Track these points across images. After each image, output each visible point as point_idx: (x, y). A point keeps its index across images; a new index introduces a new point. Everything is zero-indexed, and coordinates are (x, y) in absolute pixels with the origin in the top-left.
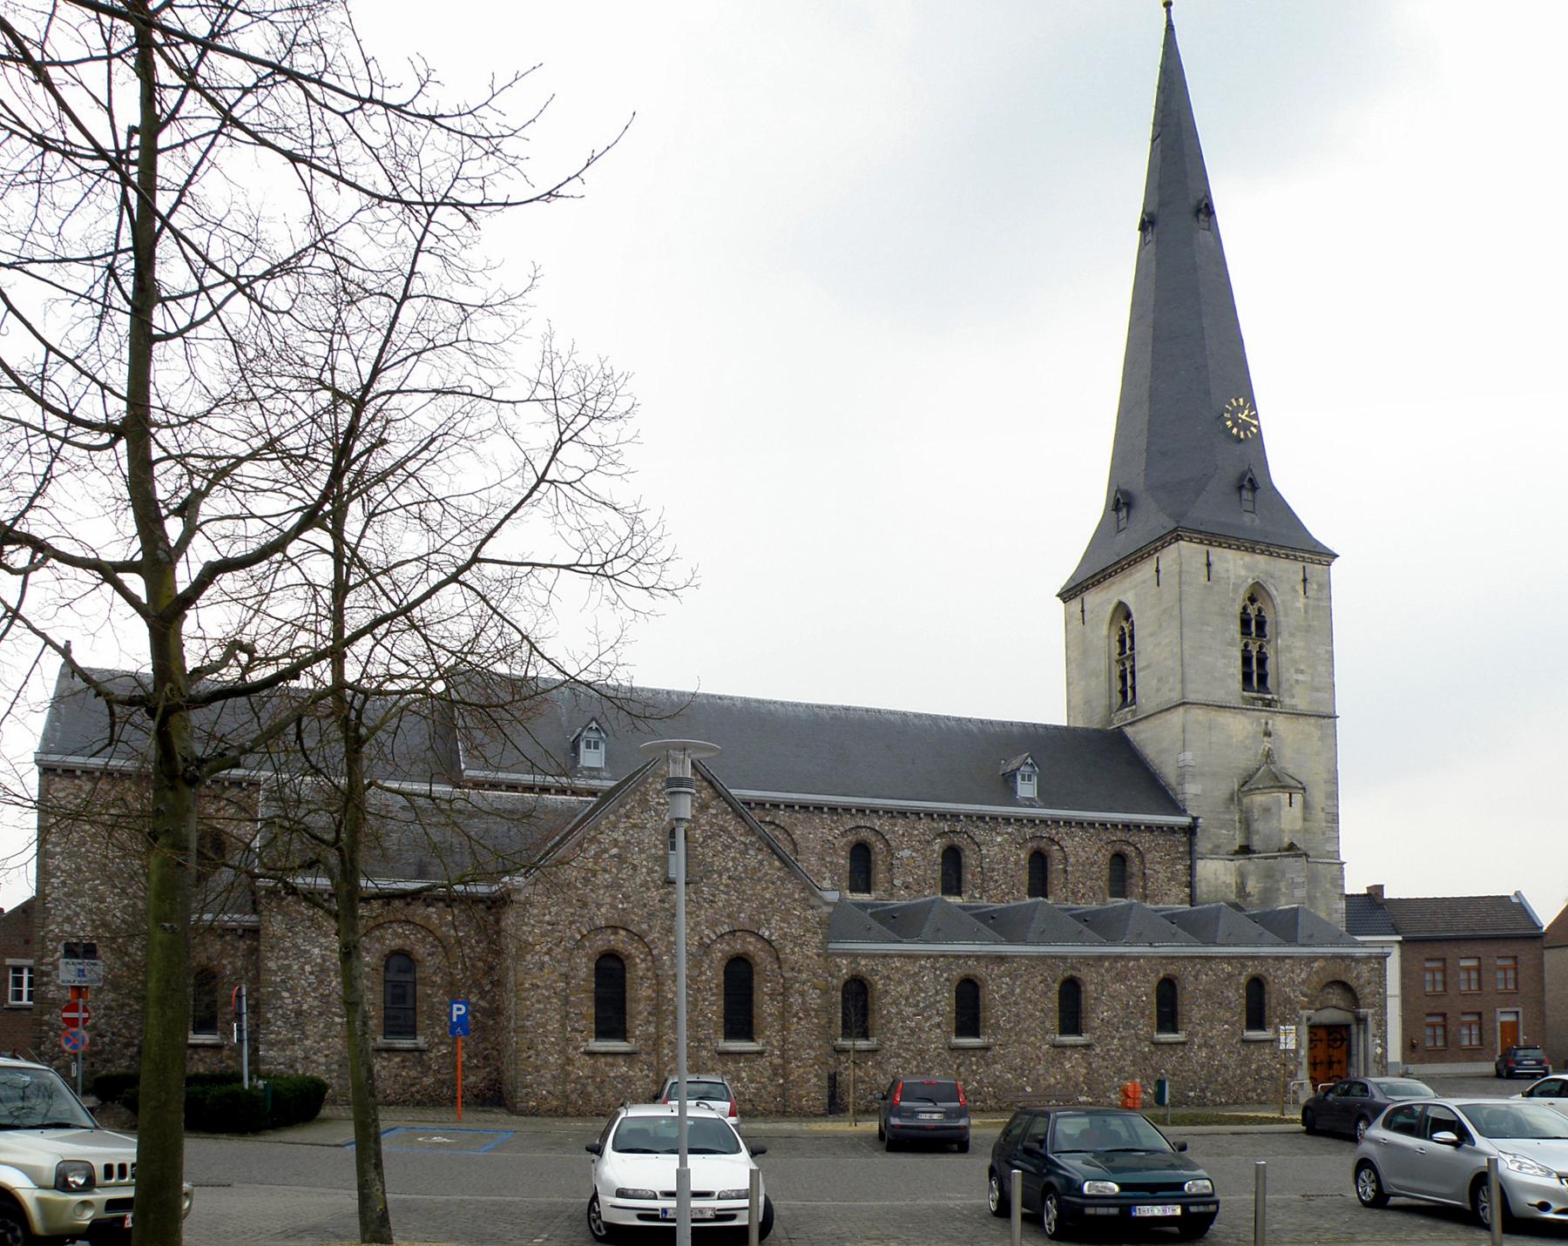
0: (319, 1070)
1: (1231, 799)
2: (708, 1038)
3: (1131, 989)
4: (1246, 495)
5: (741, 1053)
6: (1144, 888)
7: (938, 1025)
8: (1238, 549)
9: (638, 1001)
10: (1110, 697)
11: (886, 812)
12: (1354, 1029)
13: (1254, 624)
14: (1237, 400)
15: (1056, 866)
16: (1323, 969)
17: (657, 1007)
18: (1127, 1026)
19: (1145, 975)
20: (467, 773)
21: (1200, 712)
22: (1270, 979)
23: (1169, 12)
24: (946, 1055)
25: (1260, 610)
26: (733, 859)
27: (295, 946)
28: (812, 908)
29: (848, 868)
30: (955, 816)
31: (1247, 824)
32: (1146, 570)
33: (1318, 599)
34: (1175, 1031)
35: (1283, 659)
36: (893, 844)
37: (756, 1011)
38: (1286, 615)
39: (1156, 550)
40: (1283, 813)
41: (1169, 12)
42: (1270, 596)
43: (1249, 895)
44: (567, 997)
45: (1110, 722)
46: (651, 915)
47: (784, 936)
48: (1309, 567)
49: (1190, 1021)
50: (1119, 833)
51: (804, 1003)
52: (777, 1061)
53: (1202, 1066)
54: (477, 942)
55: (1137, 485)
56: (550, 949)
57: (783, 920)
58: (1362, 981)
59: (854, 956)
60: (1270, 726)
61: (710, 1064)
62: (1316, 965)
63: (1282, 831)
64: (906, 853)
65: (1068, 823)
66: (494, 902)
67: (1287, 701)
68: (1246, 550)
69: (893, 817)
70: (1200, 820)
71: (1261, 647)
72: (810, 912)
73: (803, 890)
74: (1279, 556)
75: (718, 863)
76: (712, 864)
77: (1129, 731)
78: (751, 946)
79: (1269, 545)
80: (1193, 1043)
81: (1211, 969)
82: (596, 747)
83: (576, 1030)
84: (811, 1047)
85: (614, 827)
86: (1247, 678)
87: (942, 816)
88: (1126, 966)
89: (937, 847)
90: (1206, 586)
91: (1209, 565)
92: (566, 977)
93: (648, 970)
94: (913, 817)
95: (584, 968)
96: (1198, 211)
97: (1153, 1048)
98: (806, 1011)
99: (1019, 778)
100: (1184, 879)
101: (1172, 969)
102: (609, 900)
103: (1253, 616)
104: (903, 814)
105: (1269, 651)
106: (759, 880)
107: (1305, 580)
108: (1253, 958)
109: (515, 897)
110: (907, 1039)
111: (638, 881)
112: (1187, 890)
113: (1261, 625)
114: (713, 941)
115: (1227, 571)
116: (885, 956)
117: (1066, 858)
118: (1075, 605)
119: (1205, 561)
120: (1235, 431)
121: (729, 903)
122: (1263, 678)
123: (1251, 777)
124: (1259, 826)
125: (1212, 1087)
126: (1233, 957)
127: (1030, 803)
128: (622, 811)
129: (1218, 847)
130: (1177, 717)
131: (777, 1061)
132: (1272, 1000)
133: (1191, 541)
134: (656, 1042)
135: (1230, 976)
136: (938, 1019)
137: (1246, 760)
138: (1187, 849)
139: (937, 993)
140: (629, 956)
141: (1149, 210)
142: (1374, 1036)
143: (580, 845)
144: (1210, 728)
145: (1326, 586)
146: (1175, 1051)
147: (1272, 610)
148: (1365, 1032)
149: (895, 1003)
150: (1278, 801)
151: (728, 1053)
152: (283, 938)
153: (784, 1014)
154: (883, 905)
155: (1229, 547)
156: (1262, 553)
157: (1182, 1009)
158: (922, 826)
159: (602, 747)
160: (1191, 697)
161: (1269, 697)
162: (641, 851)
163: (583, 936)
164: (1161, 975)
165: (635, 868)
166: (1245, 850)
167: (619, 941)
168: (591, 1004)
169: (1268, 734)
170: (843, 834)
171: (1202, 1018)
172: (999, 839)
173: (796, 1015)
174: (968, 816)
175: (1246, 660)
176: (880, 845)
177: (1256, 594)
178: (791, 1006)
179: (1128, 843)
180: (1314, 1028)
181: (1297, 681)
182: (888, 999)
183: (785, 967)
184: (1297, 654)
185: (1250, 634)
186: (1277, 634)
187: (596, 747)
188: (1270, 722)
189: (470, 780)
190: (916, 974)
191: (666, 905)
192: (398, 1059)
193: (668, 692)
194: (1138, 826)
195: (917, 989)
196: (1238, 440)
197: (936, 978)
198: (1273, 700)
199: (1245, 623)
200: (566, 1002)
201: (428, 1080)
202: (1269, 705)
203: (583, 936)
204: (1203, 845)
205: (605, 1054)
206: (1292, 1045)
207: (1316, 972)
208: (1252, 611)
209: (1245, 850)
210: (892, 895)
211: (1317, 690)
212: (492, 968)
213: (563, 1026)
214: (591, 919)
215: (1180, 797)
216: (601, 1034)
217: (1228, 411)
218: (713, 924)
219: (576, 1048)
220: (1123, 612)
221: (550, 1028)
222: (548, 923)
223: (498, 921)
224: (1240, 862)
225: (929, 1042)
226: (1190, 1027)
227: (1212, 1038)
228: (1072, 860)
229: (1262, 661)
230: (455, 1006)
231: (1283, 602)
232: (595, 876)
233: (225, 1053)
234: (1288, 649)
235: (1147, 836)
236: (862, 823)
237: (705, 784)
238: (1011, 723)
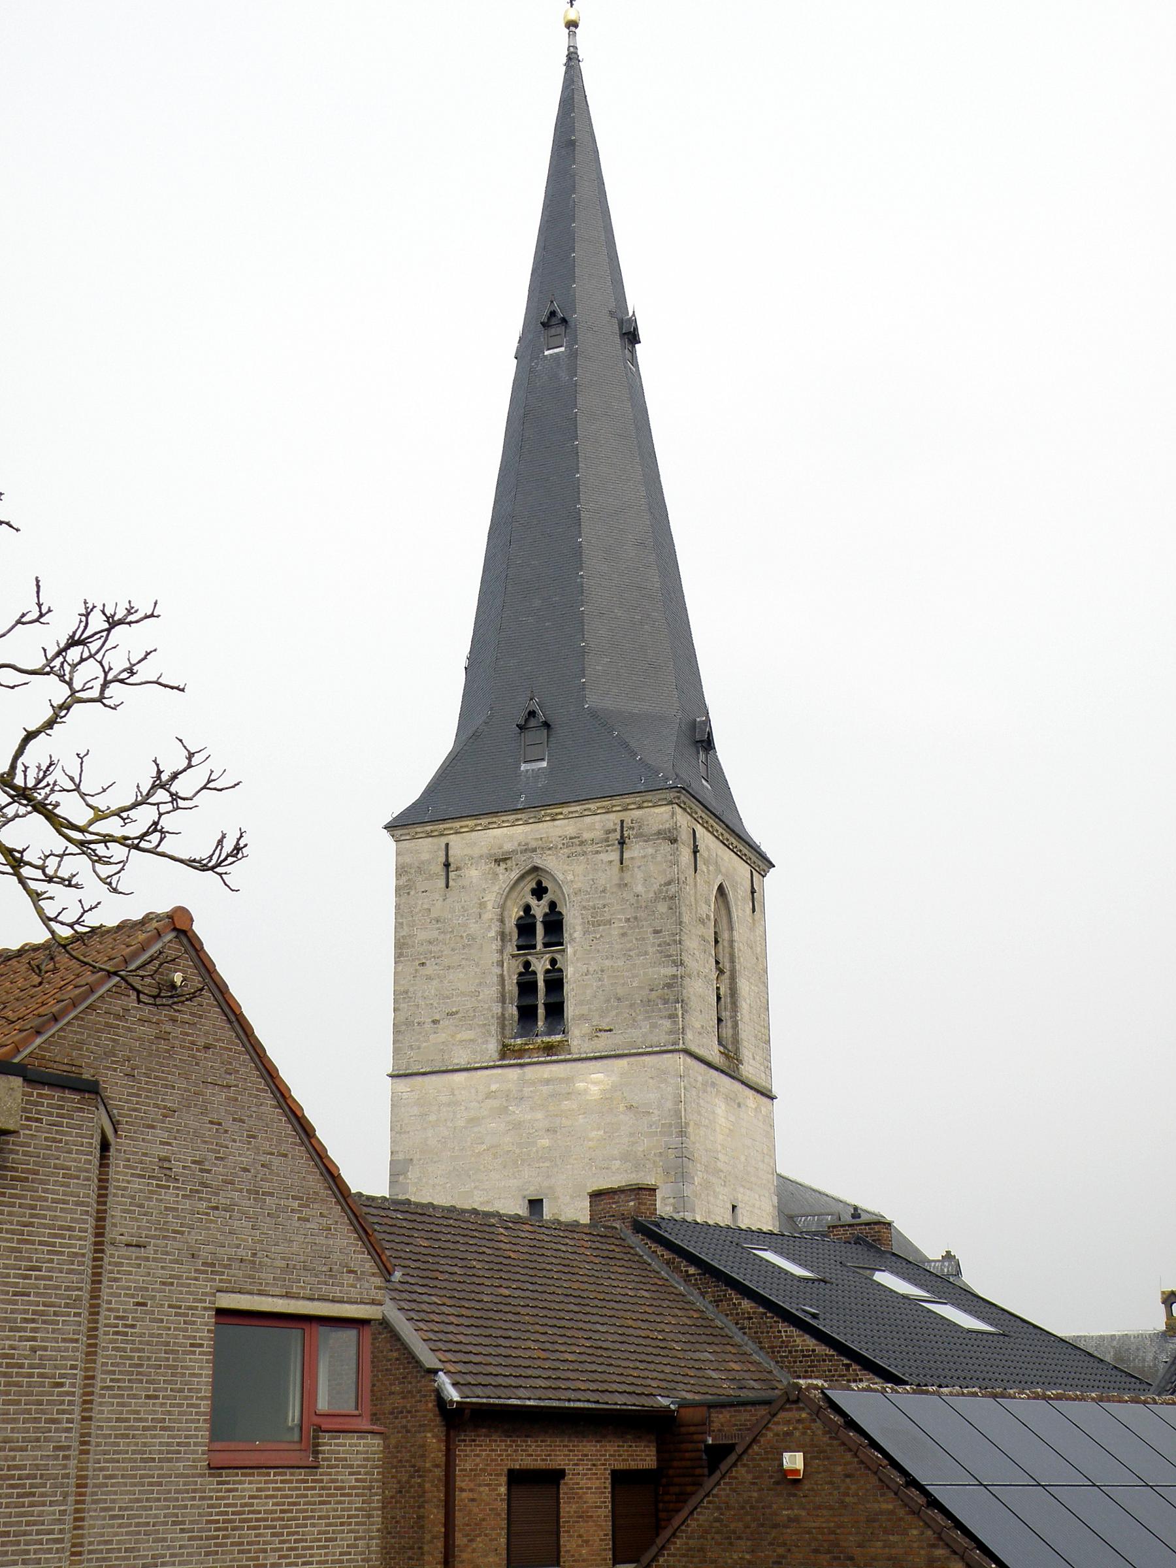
25: (553, 905)
71: (553, 962)
107: (447, 865)
175: (526, 986)
185: (534, 947)
208: (539, 909)
229: (556, 983)
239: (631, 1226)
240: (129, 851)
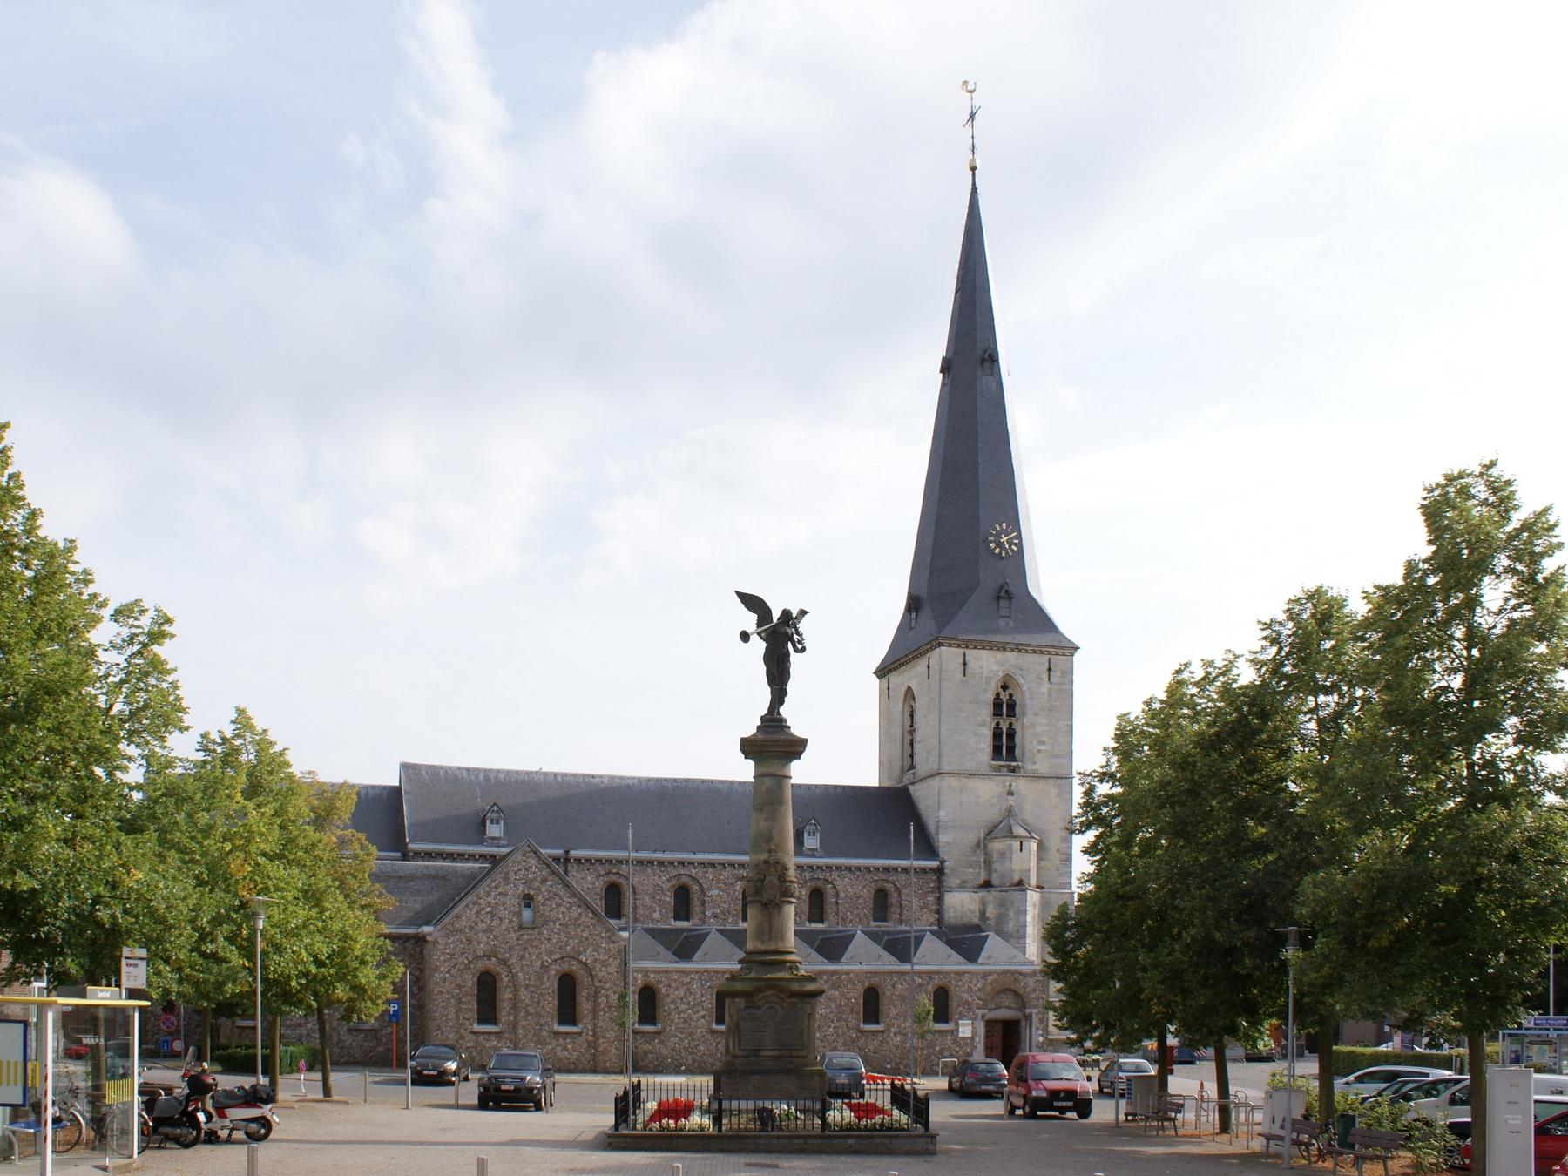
0: (600, 885)
1: (978, 845)
2: (546, 1024)
3: (843, 995)
4: (1003, 603)
5: (568, 1033)
6: (901, 914)
7: (703, 1017)
8: (991, 649)
9: (503, 1001)
10: (903, 760)
11: (700, 864)
12: (1023, 1023)
13: (1005, 706)
14: (1001, 525)
15: (830, 899)
16: (996, 980)
18: (840, 1019)
19: (854, 984)
20: (410, 846)
21: (953, 779)
22: (952, 987)
23: (974, 175)
24: (708, 1036)
25: (1011, 695)
26: (563, 913)
28: (614, 942)
29: (673, 904)
31: (988, 863)
32: (921, 665)
33: (1061, 684)
34: (878, 1023)
35: (1027, 734)
36: (705, 886)
37: (577, 1007)
38: (1031, 699)
40: (1014, 857)
41: (974, 175)
43: (988, 919)
44: (460, 999)
45: (902, 781)
46: (511, 948)
47: (595, 960)
48: (1054, 658)
49: (888, 1016)
50: (880, 875)
51: (608, 1001)
52: (591, 1039)
53: (897, 1048)
55: (923, 593)
56: (450, 970)
57: (595, 950)
58: (1028, 989)
59: (646, 972)
60: (1013, 787)
61: (548, 1040)
62: (990, 977)
63: (1012, 870)
64: (715, 892)
65: (839, 868)
66: (419, 939)
67: (1029, 767)
68: (998, 649)
69: (705, 867)
70: (947, 863)
71: (1011, 724)
72: (612, 945)
73: (607, 931)
74: (1027, 652)
75: (553, 915)
76: (549, 916)
77: (911, 788)
79: (1017, 645)
80: (890, 1032)
81: (905, 981)
82: (497, 823)
83: (464, 1018)
84: (613, 1030)
85: (488, 894)
86: (997, 750)
88: (840, 978)
89: (738, 888)
90: (962, 681)
91: (965, 664)
92: (459, 987)
93: (509, 981)
94: (720, 867)
95: (470, 981)
96: (983, 360)
97: (859, 1035)
98: (610, 1007)
99: (806, 834)
100: (934, 907)
101: (875, 981)
102: (485, 939)
103: (1005, 701)
104: (713, 865)
105: (1017, 726)
106: (579, 925)
107: (1049, 669)
108: (938, 973)
109: (428, 938)
110: (681, 1025)
111: (503, 927)
112: (936, 916)
113: (1012, 706)
115: (981, 667)
116: (667, 972)
117: (837, 894)
118: (885, 680)
119: (962, 661)
120: (997, 551)
121: (560, 940)
122: (1011, 749)
123: (995, 827)
124: (996, 866)
125: (905, 1062)
126: (923, 973)
128: (493, 884)
129: (966, 882)
130: (935, 782)
131: (591, 1039)
132: (953, 1003)
133: (950, 646)
134: (514, 1026)
135: (920, 985)
136: (703, 1013)
137: (992, 814)
138: (937, 884)
139: (702, 996)
140: (498, 973)
142: (1037, 1028)
143: (467, 906)
144: (961, 792)
145: (1068, 673)
146: (876, 1037)
148: (1031, 1026)
149: (673, 1002)
150: (1011, 847)
151: (559, 1033)
153: (594, 1012)
154: (696, 930)
155: (984, 648)
156: (1013, 650)
157: (883, 1007)
158: (727, 872)
159: (502, 822)
160: (946, 768)
161: (1014, 764)
162: (505, 909)
163: (470, 962)
164: (866, 985)
165: (501, 919)
166: (987, 885)
167: (492, 964)
168: (475, 1003)
169: (1010, 793)
170: (669, 880)
171: (898, 1014)
173: (603, 1009)
175: (997, 735)
176: (696, 887)
178: (599, 1004)
179: (888, 881)
180: (990, 1024)
181: (1039, 751)
182: (669, 1000)
183: (596, 980)
184: (1039, 729)
185: (1001, 715)
186: (1024, 714)
187: (497, 823)
188: (1014, 784)
190: (688, 983)
192: (362, 1036)
193: (555, 774)
194: (896, 869)
195: (689, 992)
196: (1000, 557)
197: (702, 986)
198: (1018, 767)
199: (997, 705)
200: (459, 1001)
201: (381, 1049)
202: (1013, 771)
203: (470, 962)
204: (951, 880)
205: (483, 1033)
206: (969, 1034)
207: (990, 984)
208: (1004, 696)
209: (987, 885)
210: (704, 923)
211: (1057, 756)
212: (419, 979)
213: (458, 1016)
214: (474, 951)
215: (936, 845)
216: (481, 1021)
217: (992, 535)
218: (550, 953)
223: (422, 951)
224: (982, 893)
225: (696, 1027)
226: (888, 1020)
227: (905, 1028)
228: (842, 895)
229: (1011, 735)
231: (1029, 688)
232: (476, 924)
234: (1033, 725)
235: (904, 876)
236: (683, 872)
238: (816, 786)
239: (331, 823)
240: (1290, 1096)
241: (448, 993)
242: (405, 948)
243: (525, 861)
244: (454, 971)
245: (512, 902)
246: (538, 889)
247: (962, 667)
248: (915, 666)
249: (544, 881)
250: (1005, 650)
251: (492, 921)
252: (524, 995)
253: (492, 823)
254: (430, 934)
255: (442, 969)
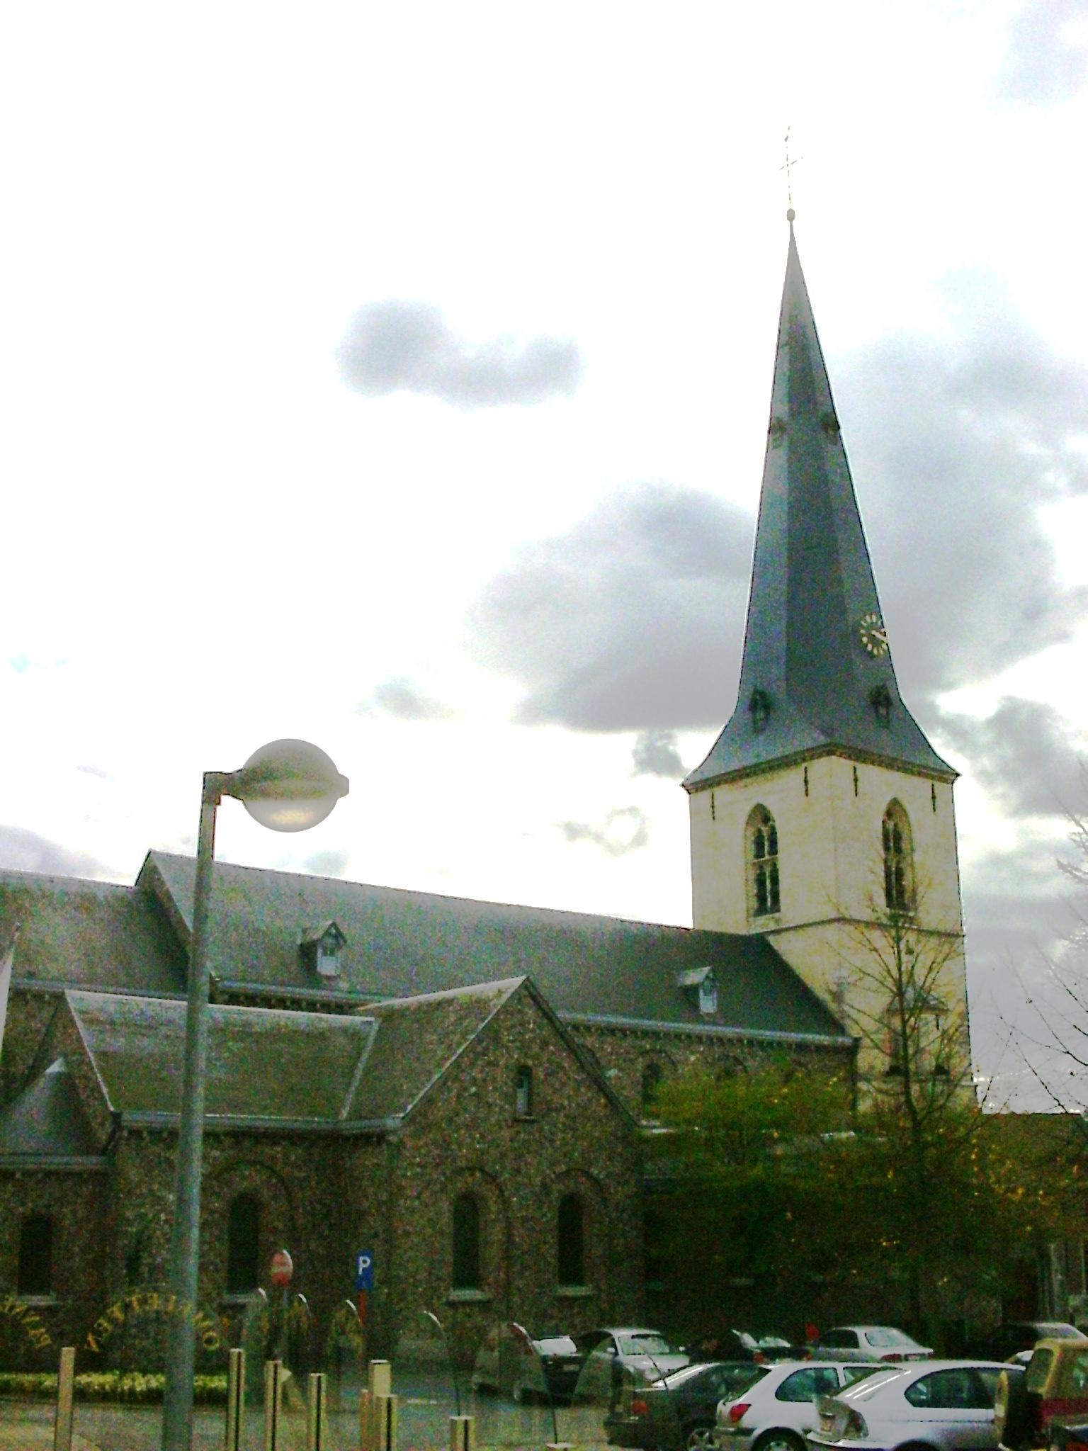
13: (894, 841)
17: (507, 1251)
25: (895, 825)
27: (151, 1191)
30: (655, 1035)
32: (793, 777)
39: (804, 760)
42: (905, 811)
54: (318, 1183)
56: (420, 1193)
71: (898, 863)
77: (772, 940)
78: (584, 1187)
87: (645, 1034)
89: (639, 1067)
94: (619, 1034)
111: (493, 1120)
112: (247, 1144)
114: (553, 1181)
118: (704, 796)
127: (712, 1020)
141: (776, 414)
147: (906, 827)
152: (139, 1185)
162: (495, 1089)
165: (490, 1106)
172: (693, 1058)
174: (667, 1034)
177: (894, 810)
186: (913, 850)
189: (223, 992)
191: (516, 1145)
196: (871, 655)
205: (464, 1304)
208: (890, 825)
213: (430, 1274)
219: (439, 1298)
220: (762, 815)
221: (418, 1277)
222: (419, 1165)
229: (775, 881)
230: (361, 1259)
233: (61, 1315)
237: (545, 1021)
241: (418, 1234)
242: (311, 1154)
243: (520, 1011)
244: (426, 1195)
245: (503, 1076)
246: (536, 1057)
247: (853, 784)
248: (772, 779)
249: (545, 1044)
250: (892, 768)
251: (477, 1107)
252: (519, 1235)
253: (325, 954)
254: (394, 1132)
255: (408, 1192)
